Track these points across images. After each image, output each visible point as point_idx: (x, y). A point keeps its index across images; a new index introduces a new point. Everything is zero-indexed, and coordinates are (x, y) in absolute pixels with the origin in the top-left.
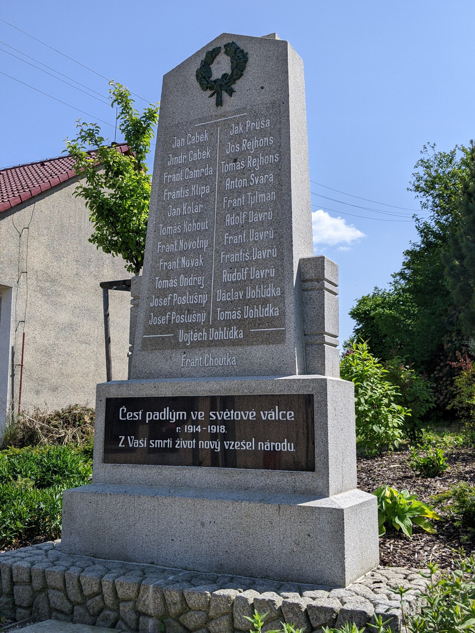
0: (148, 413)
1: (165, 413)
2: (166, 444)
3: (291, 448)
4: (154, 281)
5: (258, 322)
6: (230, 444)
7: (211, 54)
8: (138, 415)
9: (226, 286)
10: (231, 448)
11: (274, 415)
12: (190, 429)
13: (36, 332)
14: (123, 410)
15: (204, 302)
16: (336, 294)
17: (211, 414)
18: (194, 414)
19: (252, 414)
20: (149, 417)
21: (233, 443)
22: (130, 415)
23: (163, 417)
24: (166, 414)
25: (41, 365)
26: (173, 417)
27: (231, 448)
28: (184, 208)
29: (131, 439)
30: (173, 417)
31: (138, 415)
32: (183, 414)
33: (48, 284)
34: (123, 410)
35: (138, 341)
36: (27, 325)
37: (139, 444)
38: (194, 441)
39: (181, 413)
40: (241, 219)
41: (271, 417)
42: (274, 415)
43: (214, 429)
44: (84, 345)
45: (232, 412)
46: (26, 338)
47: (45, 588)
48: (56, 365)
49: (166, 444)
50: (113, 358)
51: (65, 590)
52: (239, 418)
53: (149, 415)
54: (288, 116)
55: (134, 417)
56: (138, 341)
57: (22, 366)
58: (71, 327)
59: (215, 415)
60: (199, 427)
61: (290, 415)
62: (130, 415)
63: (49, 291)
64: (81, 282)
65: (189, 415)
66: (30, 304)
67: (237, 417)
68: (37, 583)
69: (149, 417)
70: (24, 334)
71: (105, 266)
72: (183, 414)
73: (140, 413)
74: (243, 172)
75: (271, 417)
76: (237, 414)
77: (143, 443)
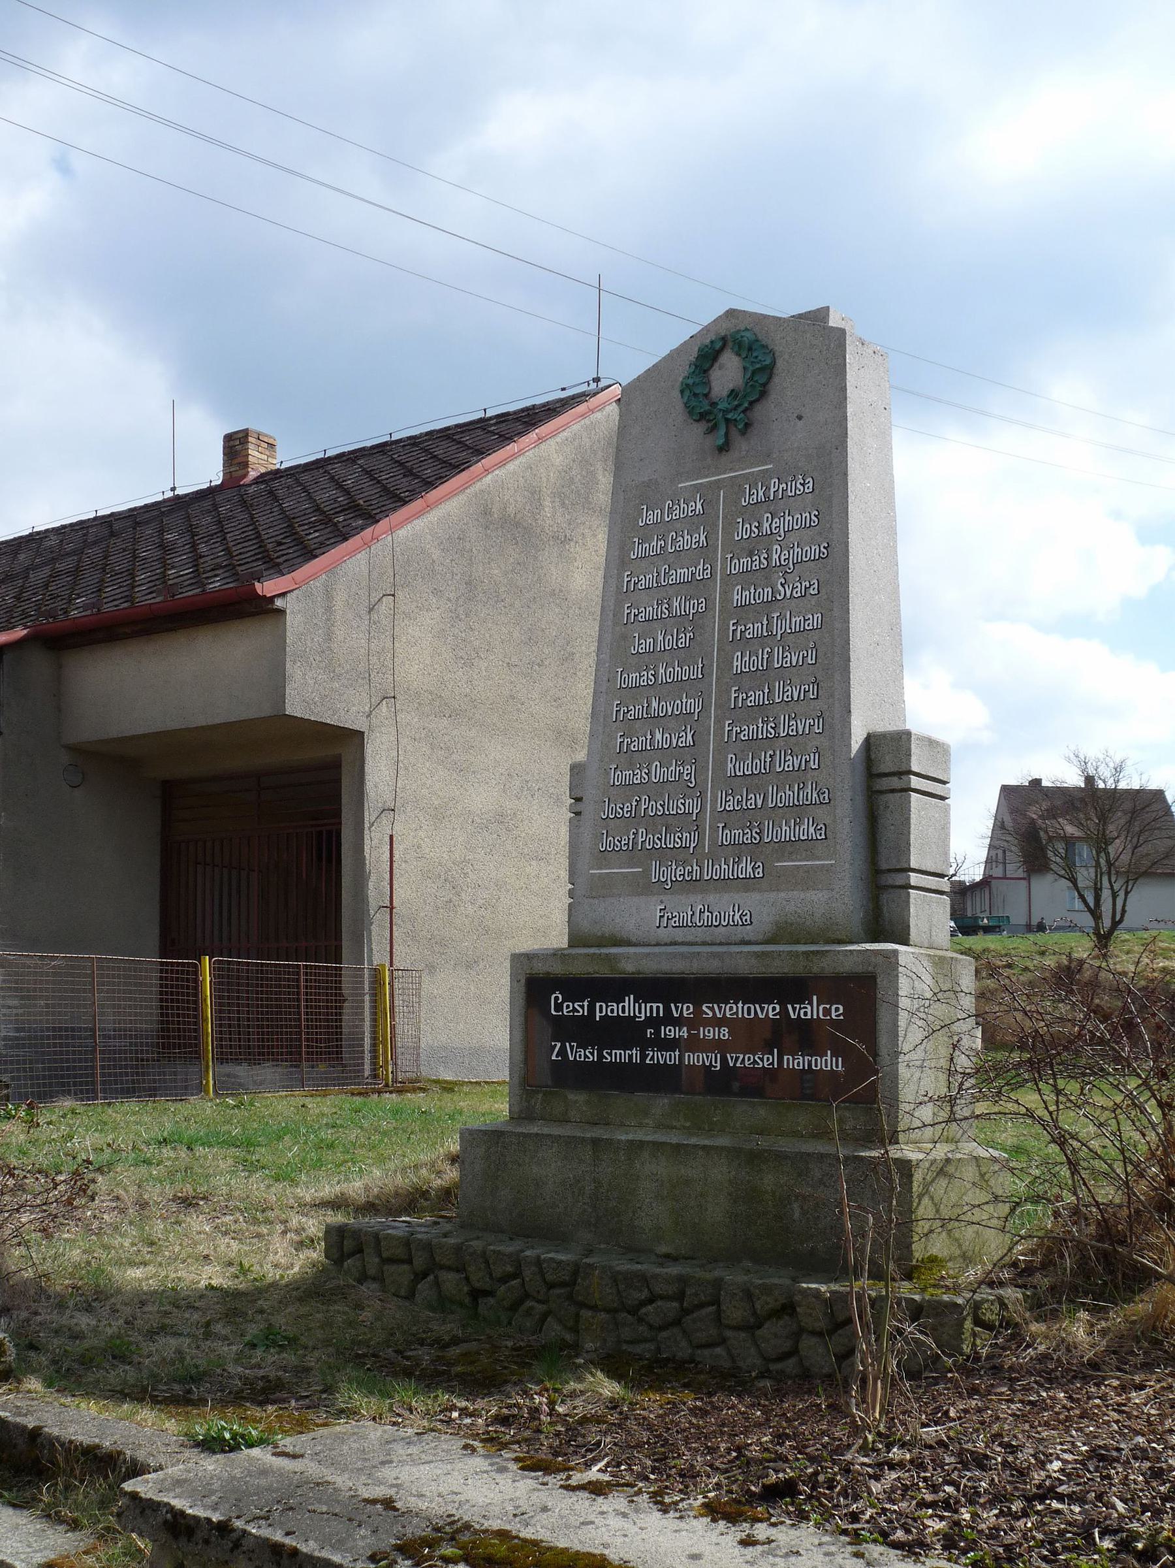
0: (598, 1005)
1: (626, 1004)
2: (631, 1057)
3: (837, 1066)
6: (737, 1058)
7: (707, 353)
8: (581, 1008)
9: (731, 784)
10: (738, 1065)
12: (669, 1032)
13: (421, 834)
14: (557, 998)
15: (695, 811)
16: (943, 798)
17: (704, 1008)
18: (677, 1008)
19: (774, 1009)
20: (601, 1011)
21: (741, 1056)
22: (568, 1007)
23: (623, 1012)
24: (629, 1007)
25: (438, 908)
26: (640, 1012)
27: (738, 1065)
28: (660, 638)
29: (572, 1047)
30: (640, 1012)
31: (581, 1008)
32: (658, 1008)
34: (557, 998)
36: (400, 818)
37: (586, 1056)
38: (677, 1053)
39: (655, 1005)
40: (758, 661)
41: (806, 1014)
43: (710, 1033)
44: (534, 863)
45: (740, 1005)
48: (470, 909)
49: (631, 1057)
52: (752, 1016)
53: (601, 1007)
54: (846, 474)
55: (575, 1010)
57: (392, 908)
59: (712, 1009)
60: (685, 1029)
61: (837, 1011)
62: (568, 1007)
63: (446, 738)
64: (522, 716)
65: (667, 1010)
67: (749, 1014)
69: (601, 1011)
70: (391, 837)
71: (580, 674)
72: (658, 1008)
73: (586, 1003)
74: (766, 574)
75: (806, 1014)
76: (749, 1008)
77: (592, 1054)
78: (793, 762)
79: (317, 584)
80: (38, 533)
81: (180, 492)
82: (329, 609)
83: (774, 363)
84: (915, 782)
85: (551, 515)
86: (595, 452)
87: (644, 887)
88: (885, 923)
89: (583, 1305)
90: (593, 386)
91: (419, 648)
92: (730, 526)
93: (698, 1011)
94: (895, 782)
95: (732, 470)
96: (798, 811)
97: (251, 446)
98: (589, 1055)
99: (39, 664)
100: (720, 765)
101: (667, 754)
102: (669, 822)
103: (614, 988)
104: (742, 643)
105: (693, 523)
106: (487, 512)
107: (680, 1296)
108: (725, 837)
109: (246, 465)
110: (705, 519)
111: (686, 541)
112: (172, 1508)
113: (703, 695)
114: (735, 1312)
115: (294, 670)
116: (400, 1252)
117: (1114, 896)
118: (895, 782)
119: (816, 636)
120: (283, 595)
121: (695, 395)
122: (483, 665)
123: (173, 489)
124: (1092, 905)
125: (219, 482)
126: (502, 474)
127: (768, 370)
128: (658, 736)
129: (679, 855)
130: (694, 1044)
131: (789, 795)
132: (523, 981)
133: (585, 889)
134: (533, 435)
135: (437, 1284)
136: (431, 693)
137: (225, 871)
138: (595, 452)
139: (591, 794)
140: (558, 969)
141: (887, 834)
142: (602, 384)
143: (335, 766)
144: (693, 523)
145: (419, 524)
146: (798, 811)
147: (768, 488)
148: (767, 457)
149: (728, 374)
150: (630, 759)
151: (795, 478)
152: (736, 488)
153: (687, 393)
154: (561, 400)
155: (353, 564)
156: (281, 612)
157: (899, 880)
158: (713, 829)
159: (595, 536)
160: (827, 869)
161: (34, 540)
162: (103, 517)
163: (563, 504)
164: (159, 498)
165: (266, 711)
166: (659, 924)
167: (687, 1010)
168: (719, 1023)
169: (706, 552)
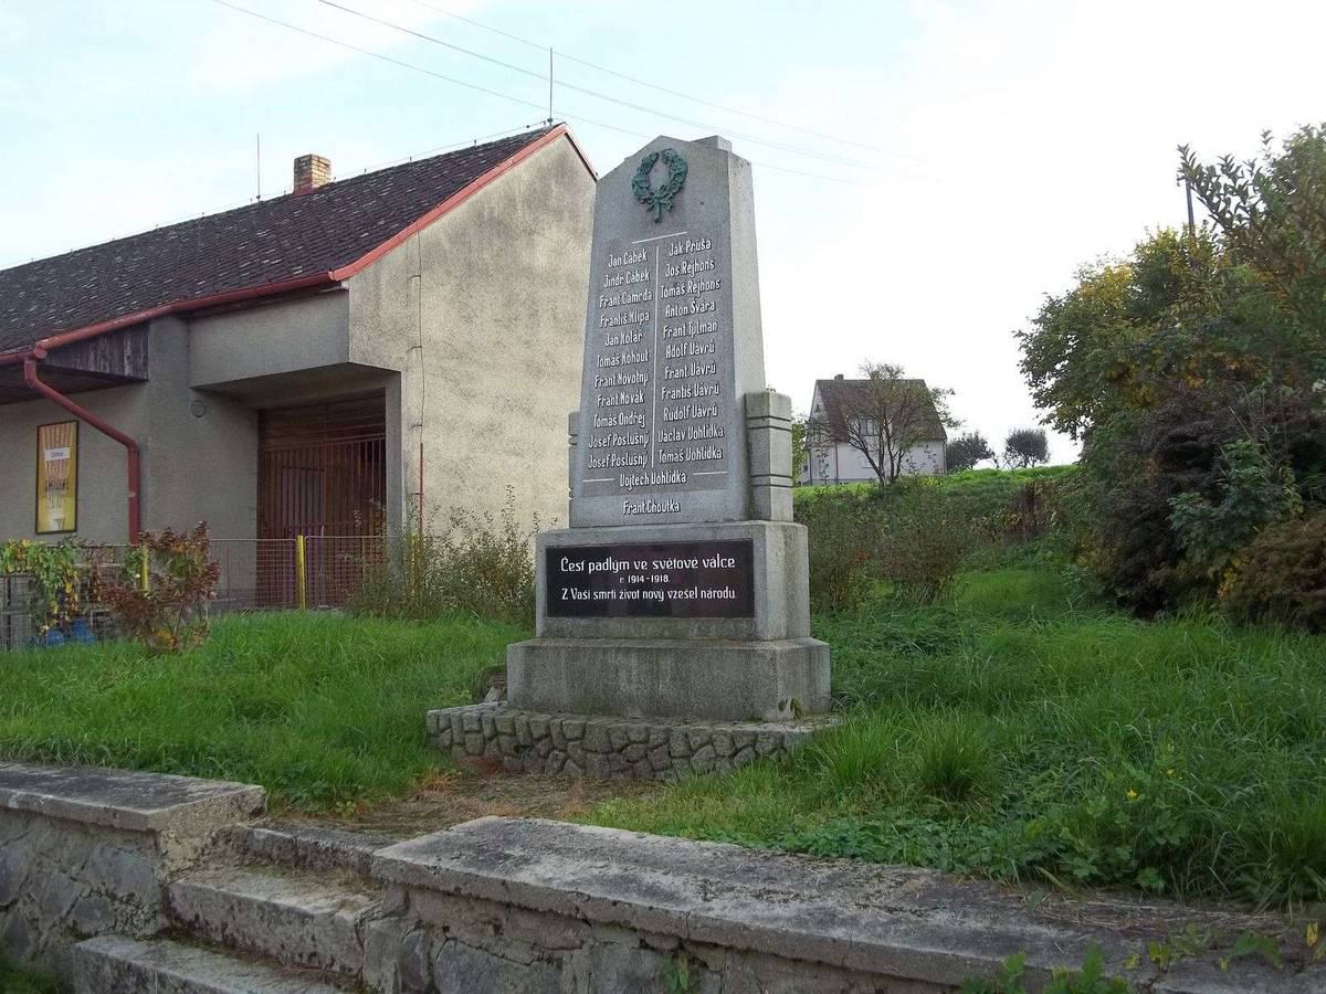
4: (593, 419)
5: (701, 463)
8: (580, 566)
11: (716, 563)
28: (623, 336)
31: (580, 566)
33: (453, 363)
35: (578, 487)
36: (425, 430)
40: (678, 352)
42: (716, 563)
46: (425, 451)
47: (496, 734)
48: (472, 492)
50: (573, 283)
51: (514, 734)
56: (578, 487)
58: (492, 429)
59: (658, 564)
61: (731, 562)
66: (429, 396)
68: (487, 731)
71: (542, 325)
78: (702, 412)
79: (370, 270)
80: (161, 229)
81: (263, 199)
82: (377, 287)
83: (686, 172)
84: (772, 422)
85: (522, 215)
86: (550, 171)
87: (616, 490)
88: (753, 509)
89: (588, 751)
90: (548, 124)
91: (435, 314)
92: (663, 268)
93: (650, 566)
94: (761, 423)
95: (663, 234)
96: (706, 442)
97: (313, 167)
98: (585, 595)
99: (175, 329)
100: (660, 413)
101: (630, 407)
102: (628, 450)
103: (599, 553)
104: (670, 339)
105: (641, 266)
106: (480, 215)
107: (646, 741)
108: (663, 458)
109: (310, 180)
110: (647, 264)
111: (636, 277)
112: (405, 862)
113: (648, 372)
114: (679, 748)
115: (355, 331)
116: (475, 726)
117: (892, 458)
118: (761, 423)
119: (714, 336)
120: (347, 279)
121: (641, 188)
122: (479, 321)
123: (258, 197)
124: (878, 465)
125: (291, 192)
126: (492, 190)
127: (684, 174)
128: (623, 397)
129: (636, 470)
130: (647, 586)
131: (700, 433)
132: (544, 551)
133: (580, 490)
134: (510, 161)
135: (499, 745)
136: (445, 342)
137: (303, 472)
138: (550, 171)
139: (583, 432)
140: (565, 542)
141: (757, 454)
142: (554, 123)
143: (381, 394)
144: (641, 266)
145: (436, 225)
146: (706, 442)
147: (685, 246)
148: (683, 226)
149: (660, 176)
150: (606, 411)
151: (700, 241)
152: (666, 244)
153: (636, 187)
154: (526, 134)
155: (396, 256)
156: (345, 291)
157: (764, 481)
158: (657, 453)
159: (550, 228)
160: (724, 476)
161: (159, 235)
162: (209, 217)
163: (529, 207)
164: (249, 203)
165: (336, 361)
166: (624, 515)
167: (643, 565)
168: (661, 572)
169: (649, 283)
